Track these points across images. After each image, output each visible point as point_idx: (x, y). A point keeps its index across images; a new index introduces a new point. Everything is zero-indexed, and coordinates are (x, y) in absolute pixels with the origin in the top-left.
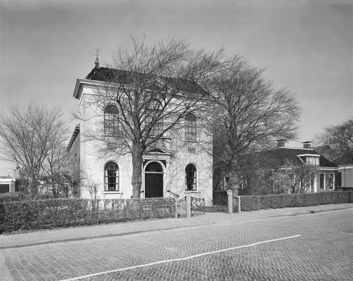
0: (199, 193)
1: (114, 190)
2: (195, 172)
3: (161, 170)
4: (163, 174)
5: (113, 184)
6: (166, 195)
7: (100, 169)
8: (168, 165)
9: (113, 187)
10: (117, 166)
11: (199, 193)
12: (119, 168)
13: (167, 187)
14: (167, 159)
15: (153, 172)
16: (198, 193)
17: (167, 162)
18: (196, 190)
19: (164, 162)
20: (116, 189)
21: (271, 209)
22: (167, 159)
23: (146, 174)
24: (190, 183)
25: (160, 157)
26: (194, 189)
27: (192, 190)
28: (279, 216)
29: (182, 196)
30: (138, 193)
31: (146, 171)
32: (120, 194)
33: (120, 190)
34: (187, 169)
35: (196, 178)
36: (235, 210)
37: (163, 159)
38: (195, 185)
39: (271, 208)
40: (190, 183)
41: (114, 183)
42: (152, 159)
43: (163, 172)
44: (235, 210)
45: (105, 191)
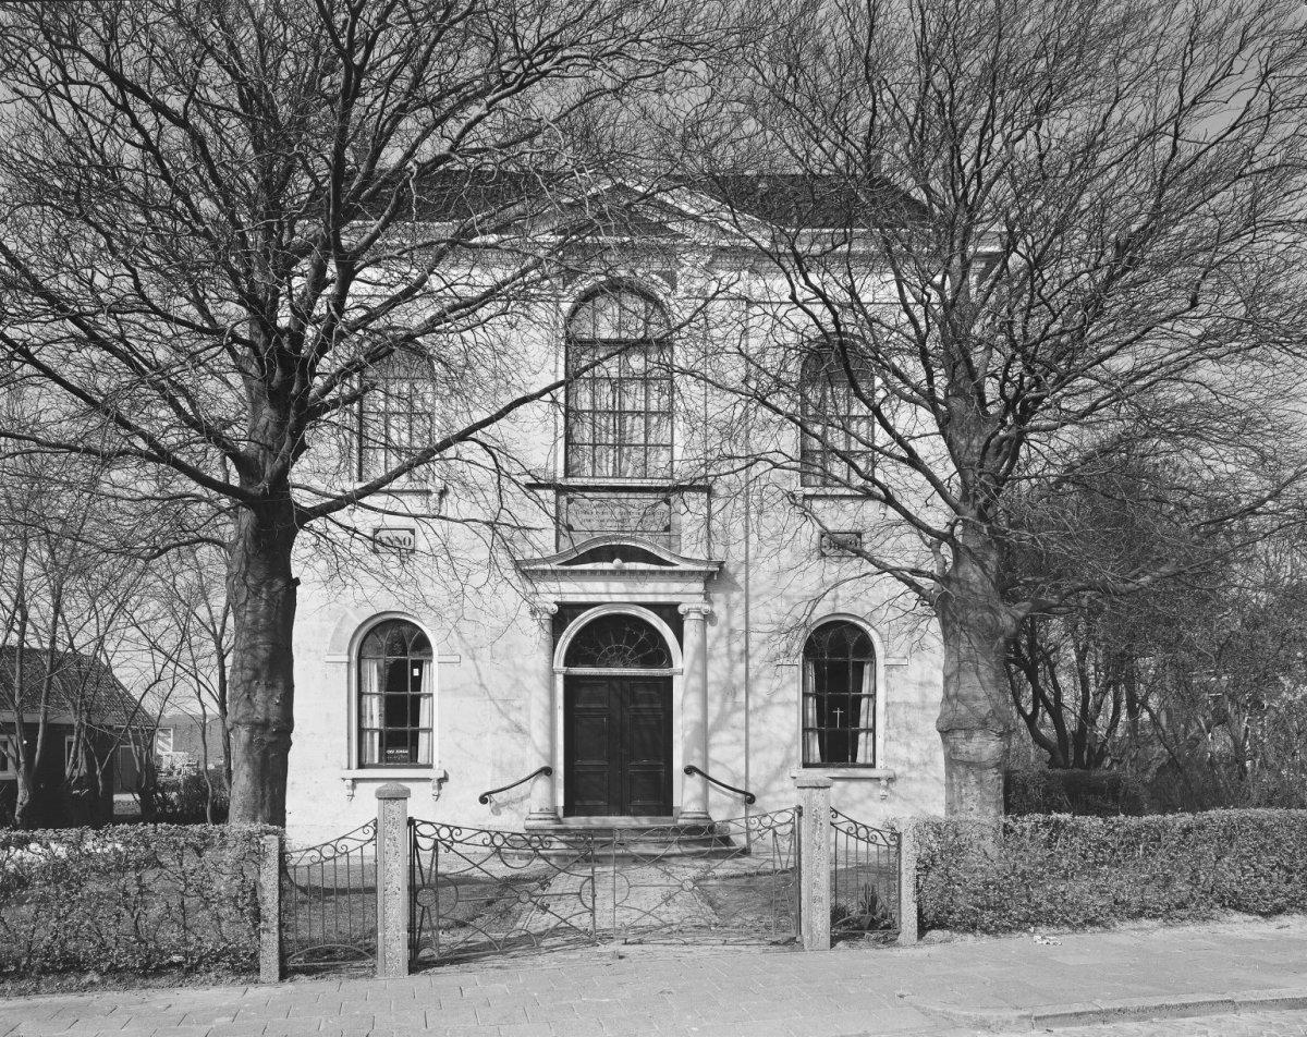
0: (884, 782)
1: (412, 760)
2: (867, 668)
3: (661, 655)
4: (669, 680)
5: (405, 732)
6: (686, 794)
7: (329, 658)
8: (690, 628)
9: (402, 745)
10: (422, 643)
11: (884, 782)
12: (431, 654)
13: (687, 755)
14: (688, 596)
15: (625, 666)
16: (878, 779)
17: (688, 613)
18: (873, 766)
19: (671, 613)
20: (422, 759)
21: (1237, 917)
22: (688, 596)
23: (568, 679)
24: (837, 729)
25: (650, 586)
26: (860, 759)
27: (854, 767)
28: (1168, 1007)
29: (781, 798)
30: (249, 784)
31: (567, 663)
32: (431, 784)
33: (879, 763)
34: (811, 650)
35: (872, 696)
36: (285, 973)
37: (662, 599)
38: (870, 736)
39: (1237, 908)
40: (837, 729)
41: (408, 728)
42: (606, 599)
43: (670, 665)
44: (285, 973)
45: (361, 766)
